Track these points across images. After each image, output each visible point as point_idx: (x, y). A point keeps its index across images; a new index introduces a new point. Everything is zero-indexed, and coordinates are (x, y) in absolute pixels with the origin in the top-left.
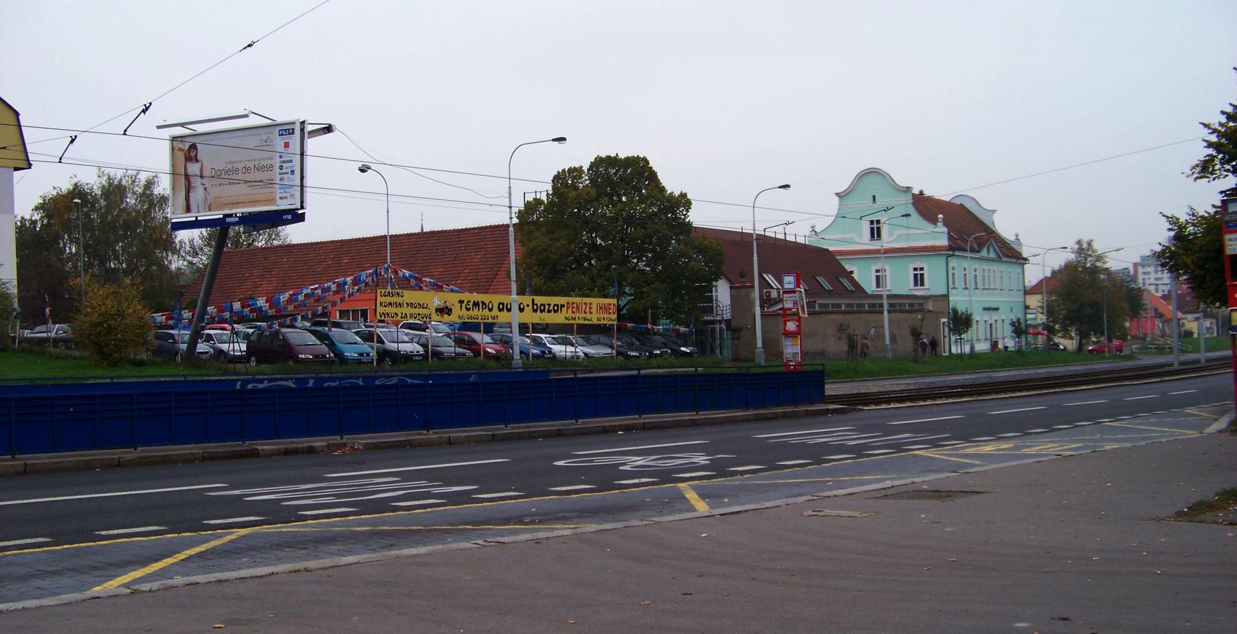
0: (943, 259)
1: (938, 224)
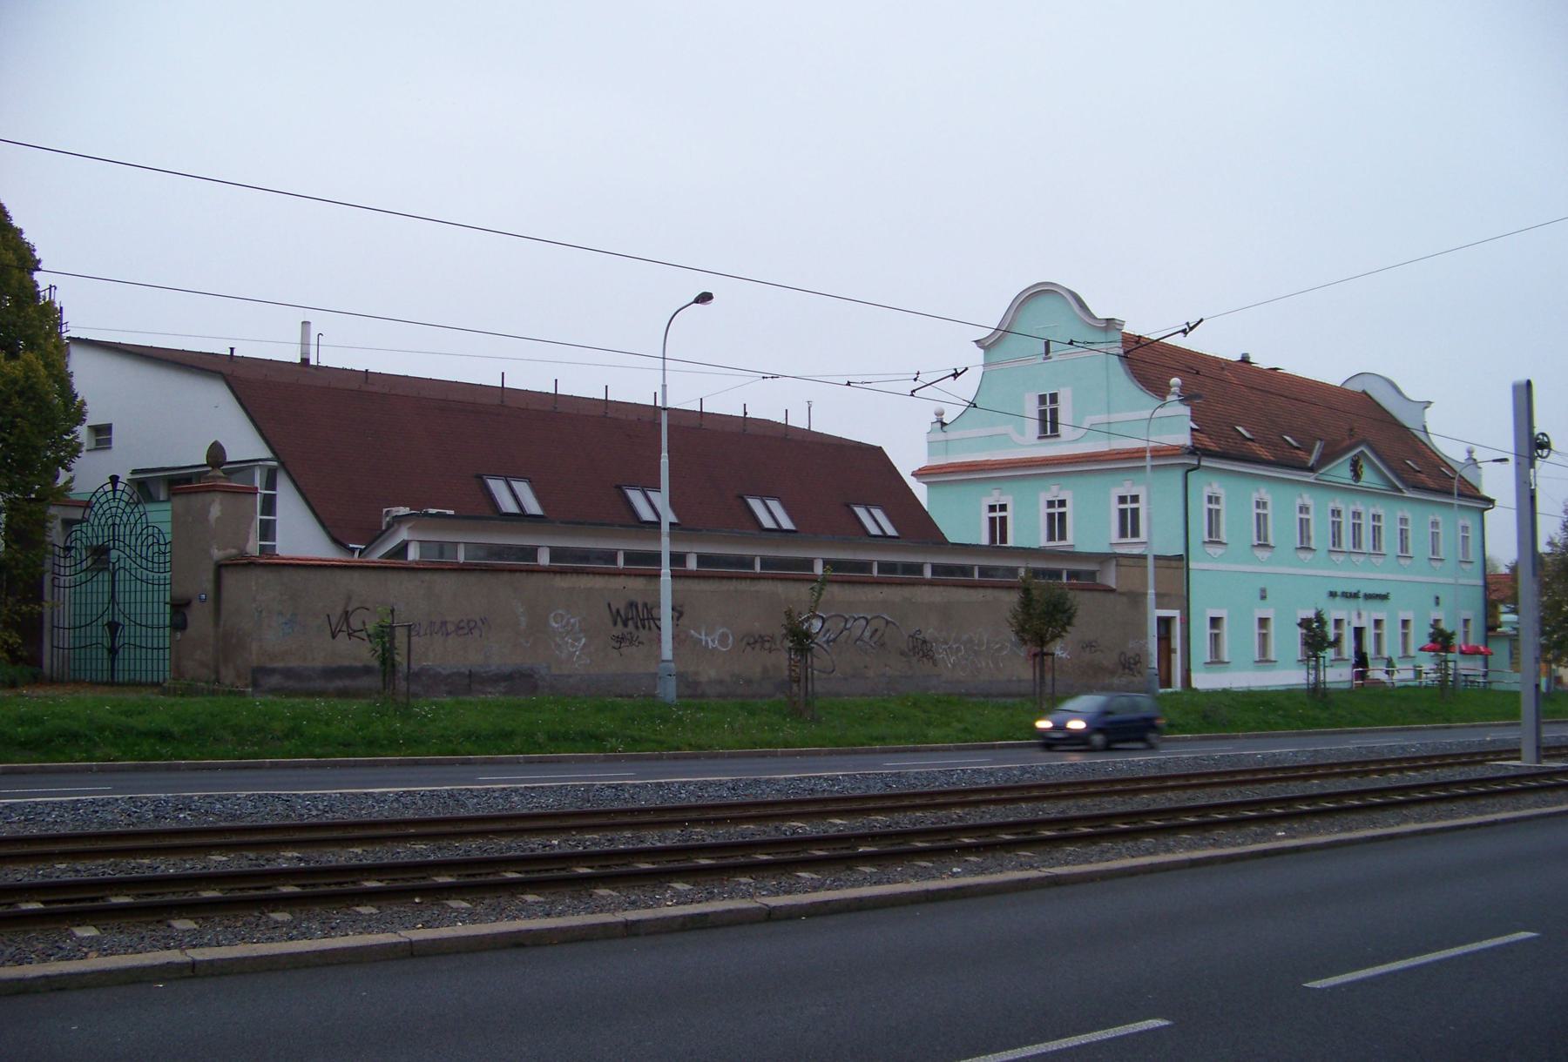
0: (1176, 477)
1: (1169, 398)
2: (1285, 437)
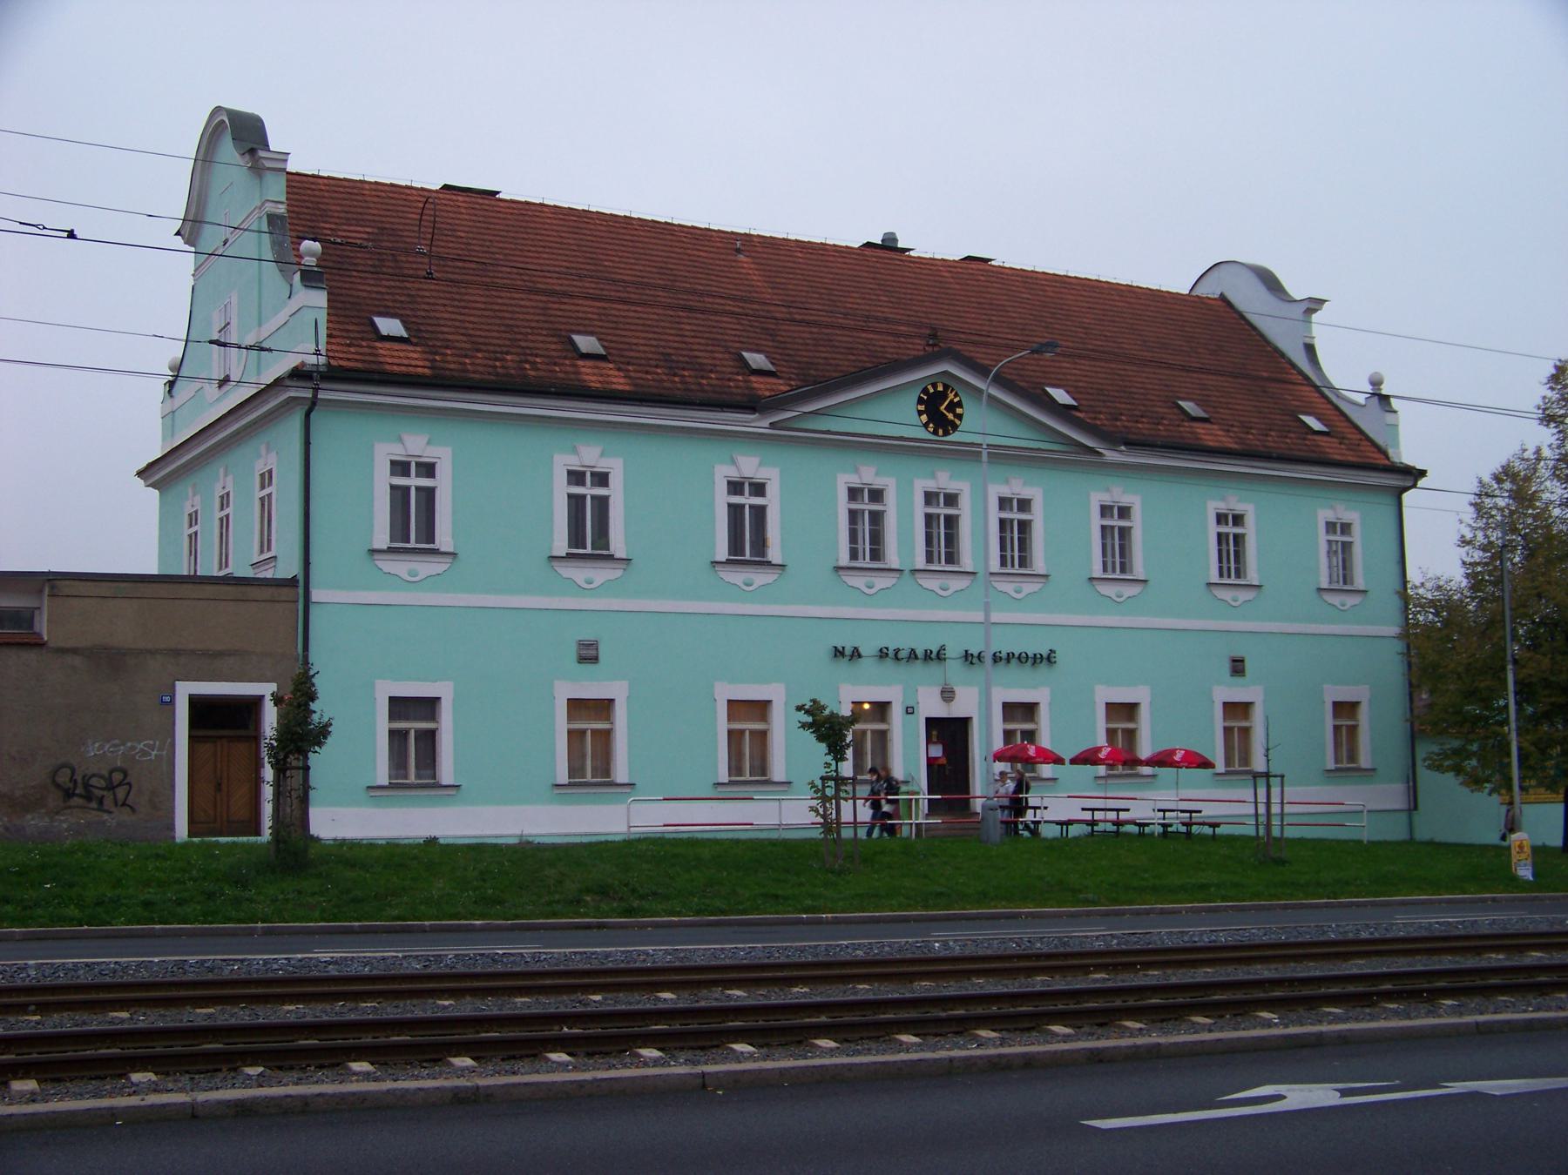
2: (1305, 418)
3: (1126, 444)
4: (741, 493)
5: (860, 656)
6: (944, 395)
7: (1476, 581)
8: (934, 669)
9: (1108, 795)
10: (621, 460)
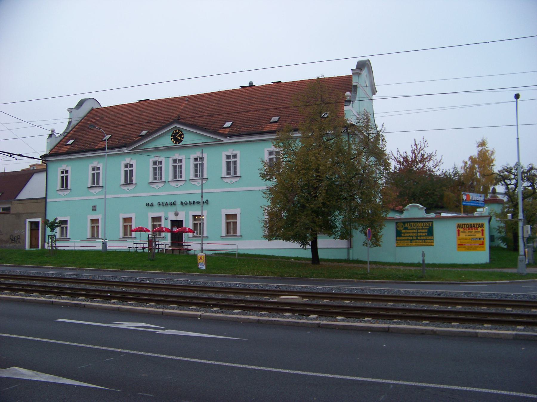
3: (229, 136)
4: (127, 167)
5: (153, 205)
6: (178, 133)
7: (478, 155)
8: (173, 207)
9: (188, 242)
10: (239, 151)
